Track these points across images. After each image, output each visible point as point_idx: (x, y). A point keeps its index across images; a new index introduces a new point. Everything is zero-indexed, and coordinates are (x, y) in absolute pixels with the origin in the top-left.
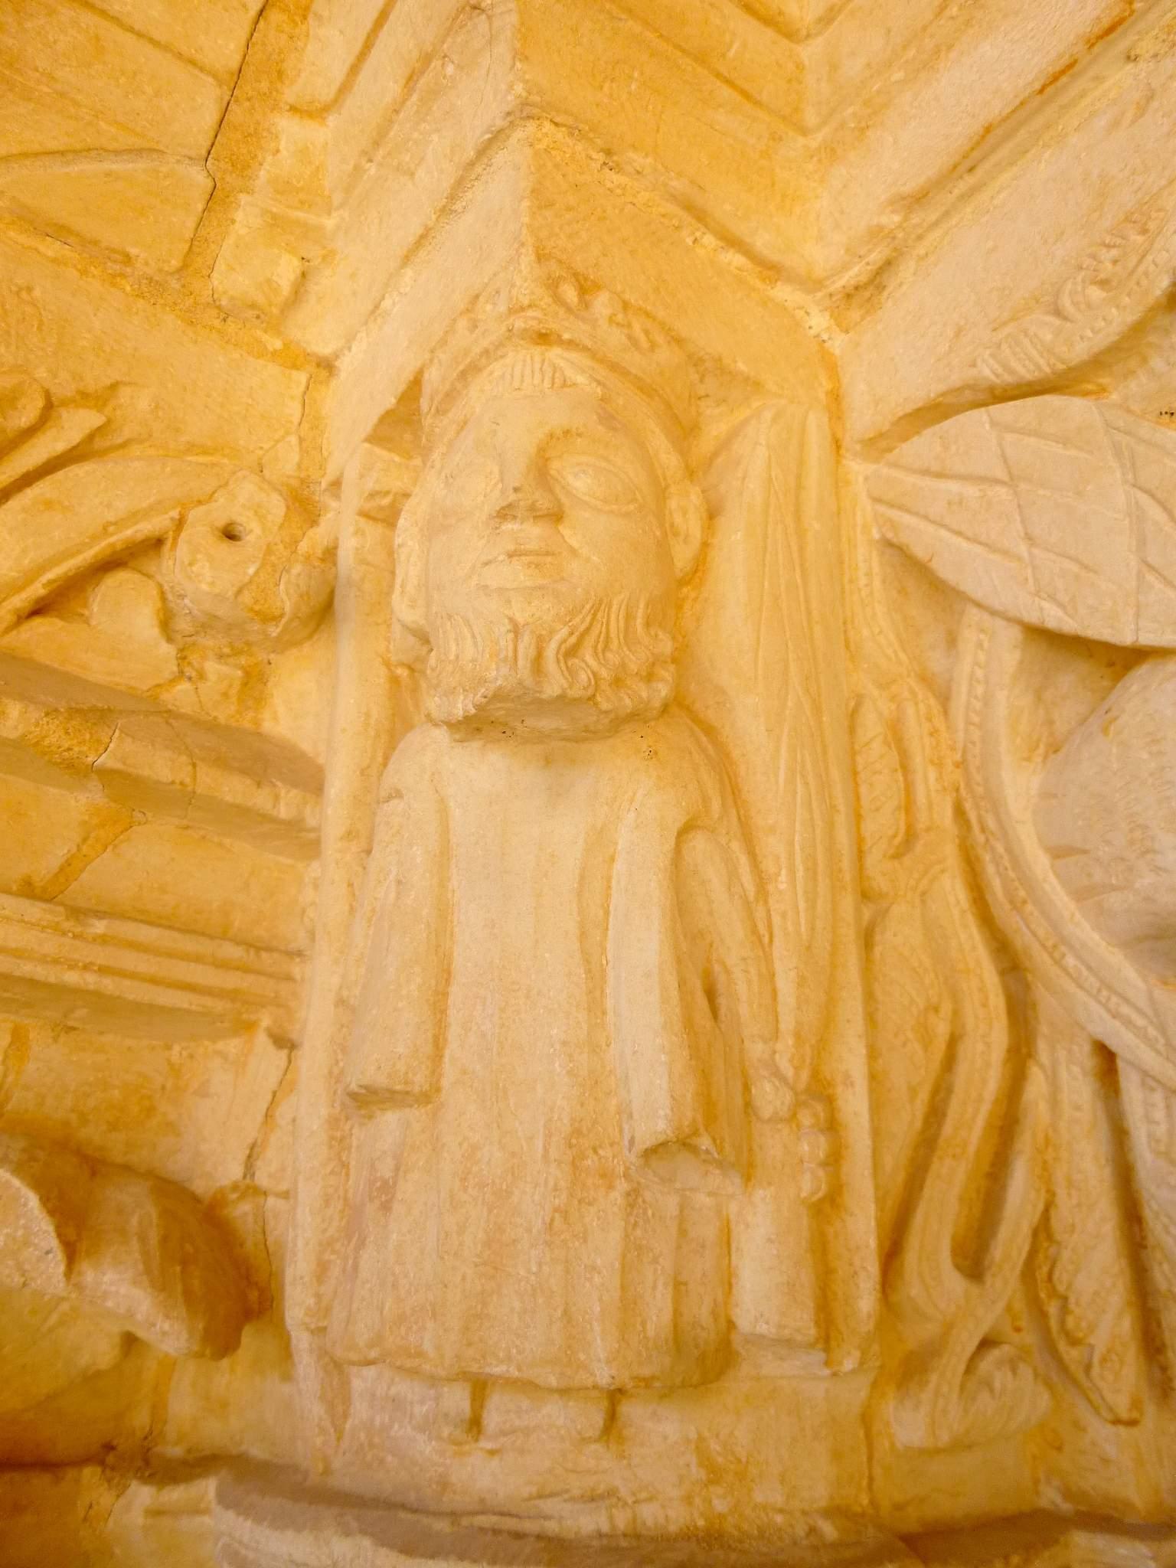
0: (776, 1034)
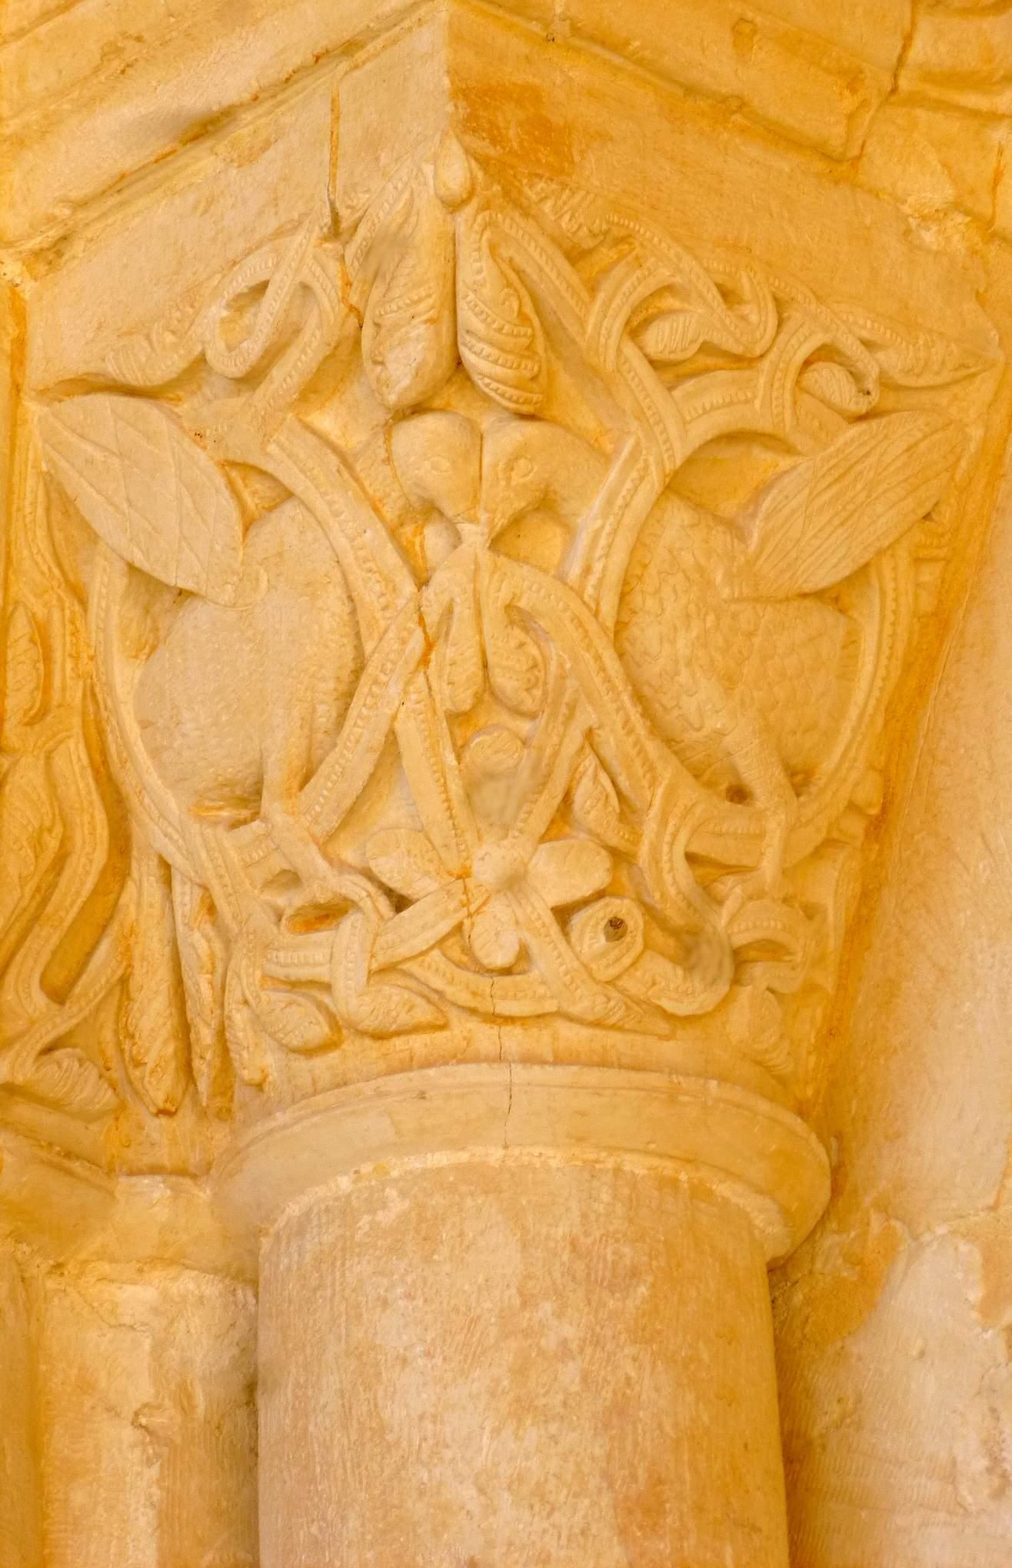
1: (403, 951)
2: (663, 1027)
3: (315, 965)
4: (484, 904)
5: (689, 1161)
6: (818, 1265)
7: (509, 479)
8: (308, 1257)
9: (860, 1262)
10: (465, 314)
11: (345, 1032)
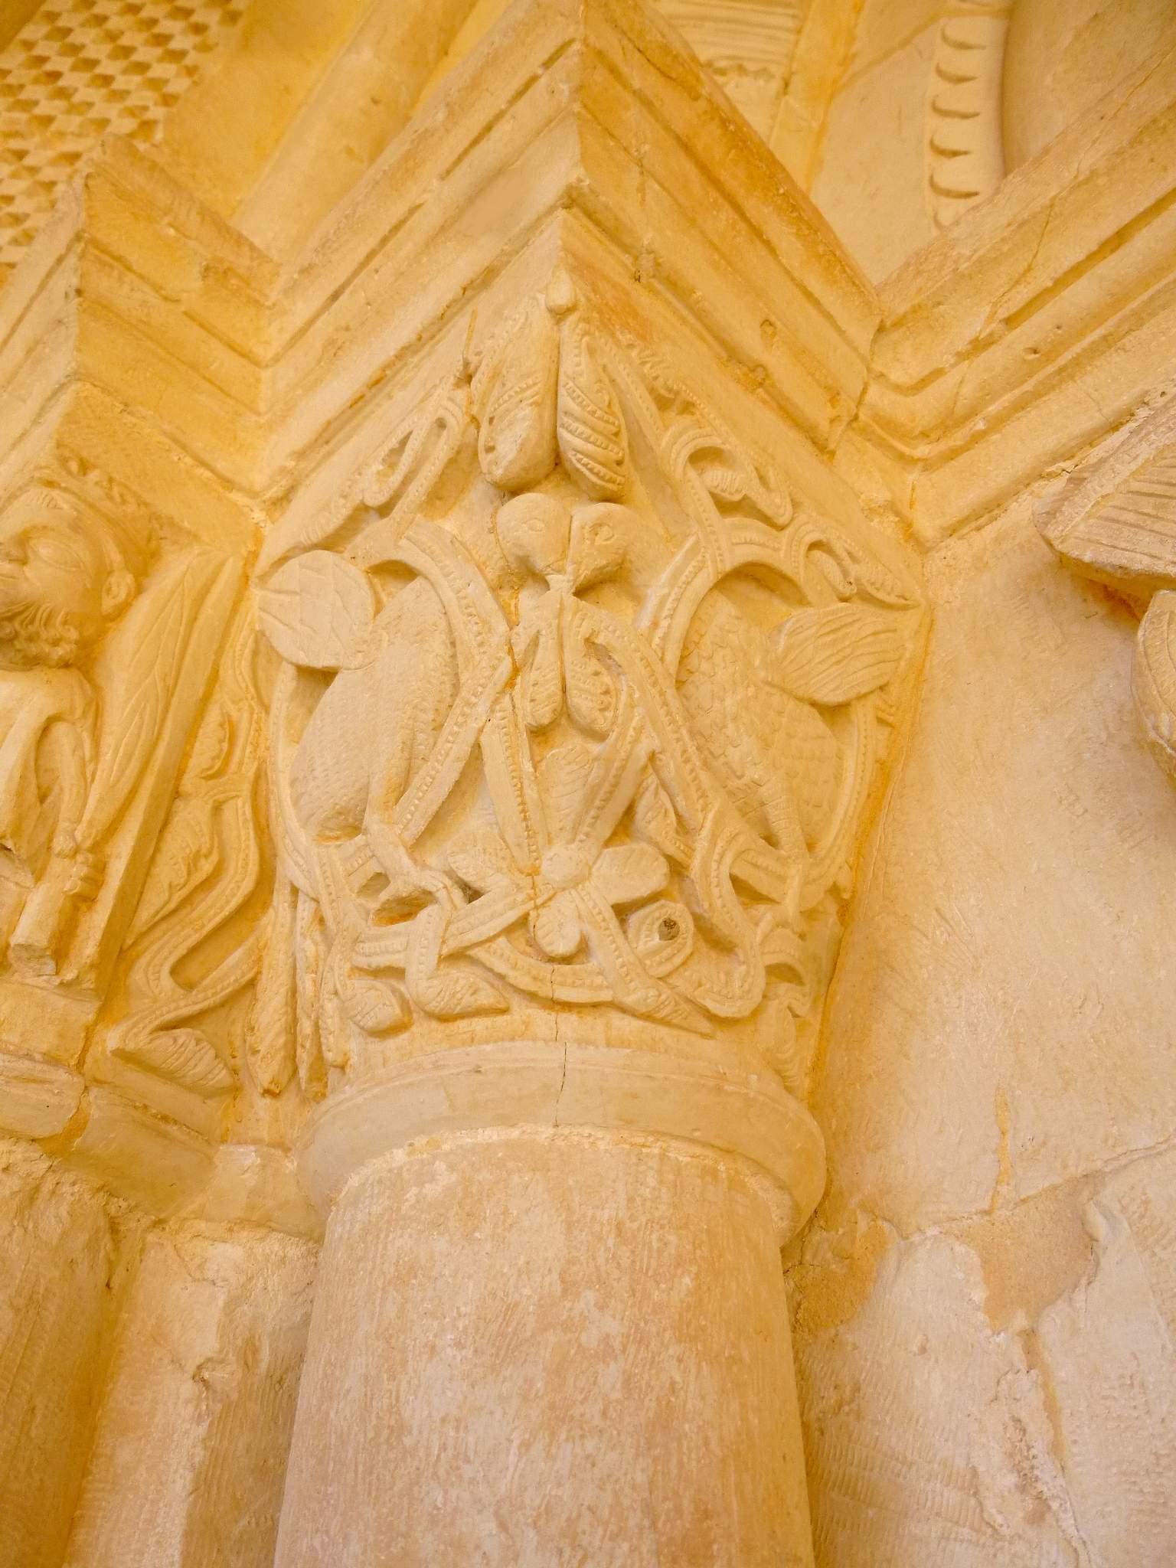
0: (79, 821)
1: (473, 937)
2: (705, 1026)
3: (393, 953)
4: (550, 899)
5: (728, 1152)
6: (808, 1257)
7: (593, 541)
8: (358, 1226)
9: (850, 1257)
10: (565, 401)
11: (415, 1015)
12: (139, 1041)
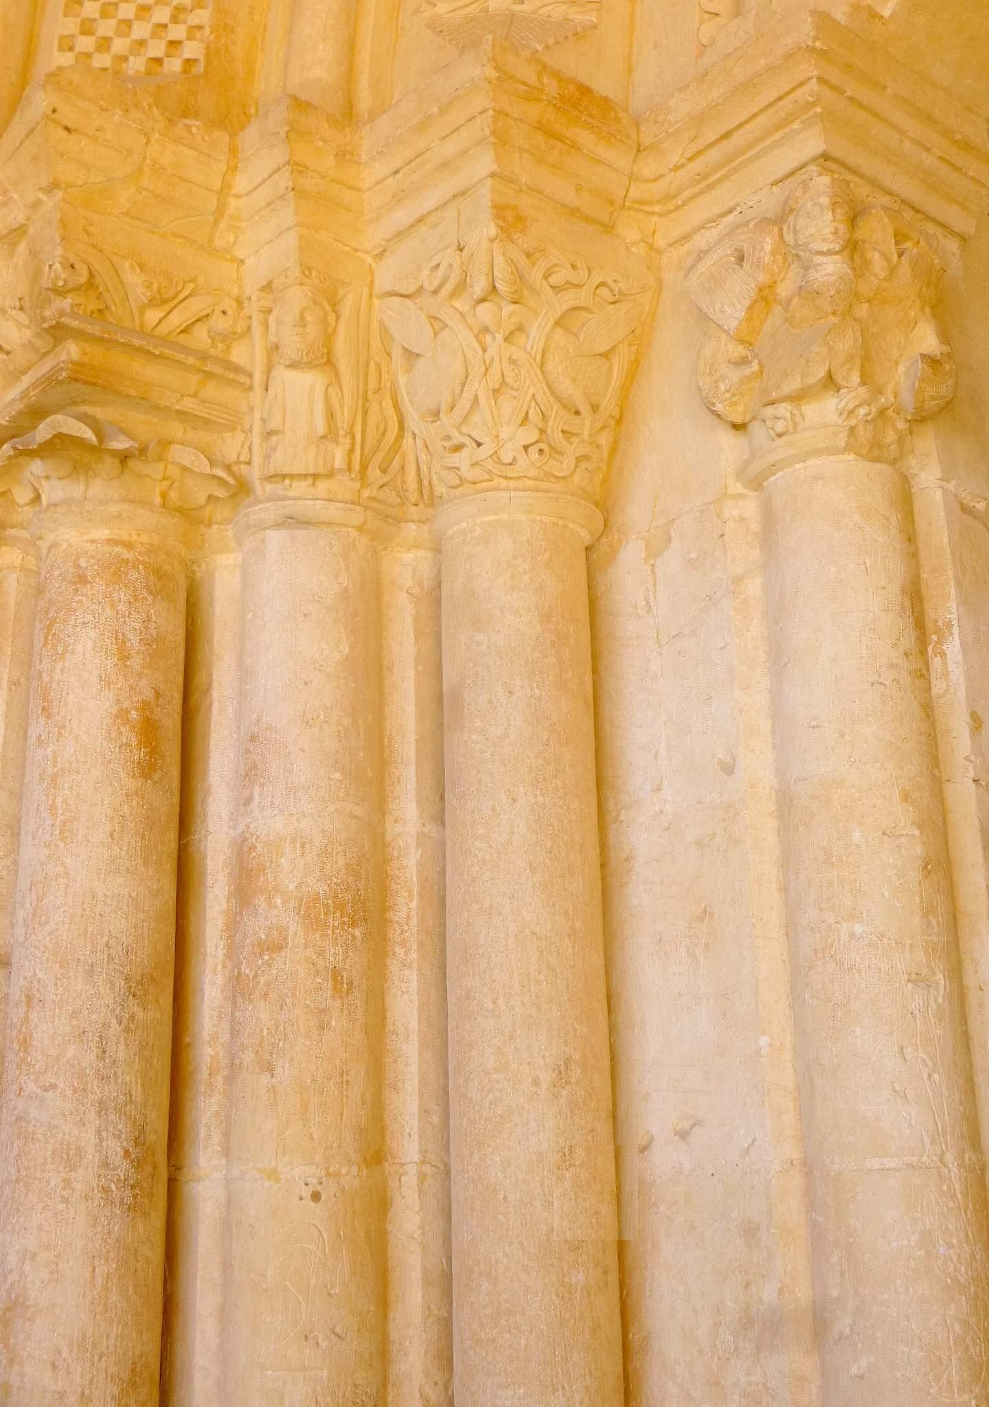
2: (554, 480)
10: (497, 274)
12: (375, 493)
